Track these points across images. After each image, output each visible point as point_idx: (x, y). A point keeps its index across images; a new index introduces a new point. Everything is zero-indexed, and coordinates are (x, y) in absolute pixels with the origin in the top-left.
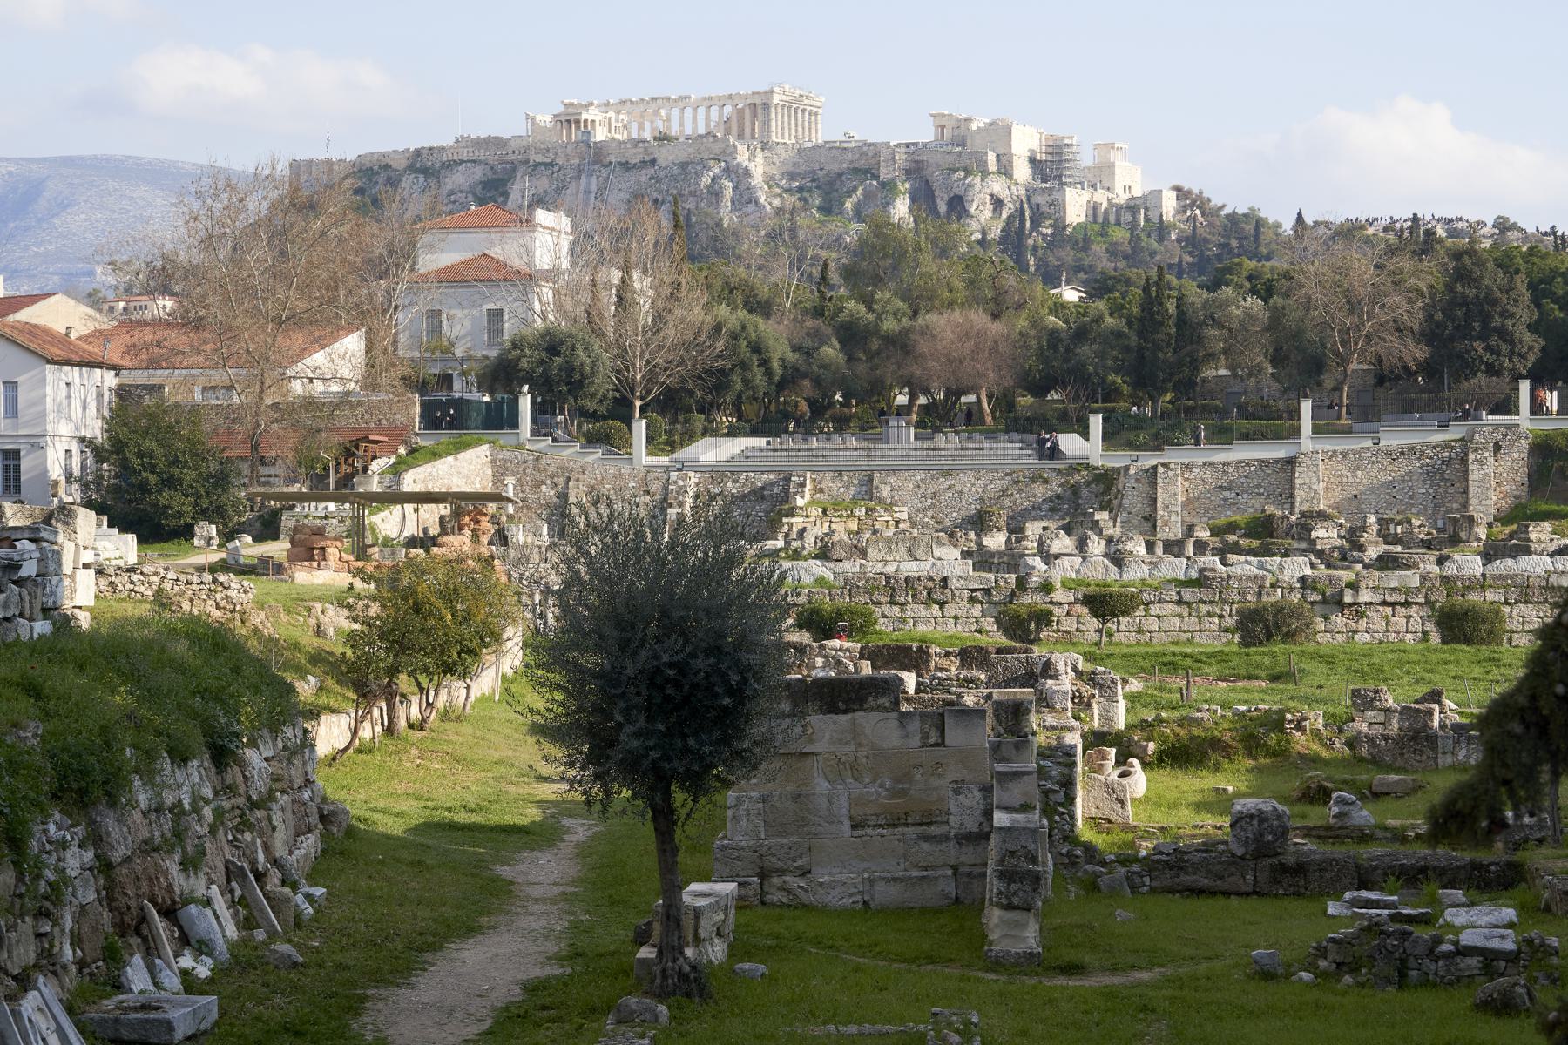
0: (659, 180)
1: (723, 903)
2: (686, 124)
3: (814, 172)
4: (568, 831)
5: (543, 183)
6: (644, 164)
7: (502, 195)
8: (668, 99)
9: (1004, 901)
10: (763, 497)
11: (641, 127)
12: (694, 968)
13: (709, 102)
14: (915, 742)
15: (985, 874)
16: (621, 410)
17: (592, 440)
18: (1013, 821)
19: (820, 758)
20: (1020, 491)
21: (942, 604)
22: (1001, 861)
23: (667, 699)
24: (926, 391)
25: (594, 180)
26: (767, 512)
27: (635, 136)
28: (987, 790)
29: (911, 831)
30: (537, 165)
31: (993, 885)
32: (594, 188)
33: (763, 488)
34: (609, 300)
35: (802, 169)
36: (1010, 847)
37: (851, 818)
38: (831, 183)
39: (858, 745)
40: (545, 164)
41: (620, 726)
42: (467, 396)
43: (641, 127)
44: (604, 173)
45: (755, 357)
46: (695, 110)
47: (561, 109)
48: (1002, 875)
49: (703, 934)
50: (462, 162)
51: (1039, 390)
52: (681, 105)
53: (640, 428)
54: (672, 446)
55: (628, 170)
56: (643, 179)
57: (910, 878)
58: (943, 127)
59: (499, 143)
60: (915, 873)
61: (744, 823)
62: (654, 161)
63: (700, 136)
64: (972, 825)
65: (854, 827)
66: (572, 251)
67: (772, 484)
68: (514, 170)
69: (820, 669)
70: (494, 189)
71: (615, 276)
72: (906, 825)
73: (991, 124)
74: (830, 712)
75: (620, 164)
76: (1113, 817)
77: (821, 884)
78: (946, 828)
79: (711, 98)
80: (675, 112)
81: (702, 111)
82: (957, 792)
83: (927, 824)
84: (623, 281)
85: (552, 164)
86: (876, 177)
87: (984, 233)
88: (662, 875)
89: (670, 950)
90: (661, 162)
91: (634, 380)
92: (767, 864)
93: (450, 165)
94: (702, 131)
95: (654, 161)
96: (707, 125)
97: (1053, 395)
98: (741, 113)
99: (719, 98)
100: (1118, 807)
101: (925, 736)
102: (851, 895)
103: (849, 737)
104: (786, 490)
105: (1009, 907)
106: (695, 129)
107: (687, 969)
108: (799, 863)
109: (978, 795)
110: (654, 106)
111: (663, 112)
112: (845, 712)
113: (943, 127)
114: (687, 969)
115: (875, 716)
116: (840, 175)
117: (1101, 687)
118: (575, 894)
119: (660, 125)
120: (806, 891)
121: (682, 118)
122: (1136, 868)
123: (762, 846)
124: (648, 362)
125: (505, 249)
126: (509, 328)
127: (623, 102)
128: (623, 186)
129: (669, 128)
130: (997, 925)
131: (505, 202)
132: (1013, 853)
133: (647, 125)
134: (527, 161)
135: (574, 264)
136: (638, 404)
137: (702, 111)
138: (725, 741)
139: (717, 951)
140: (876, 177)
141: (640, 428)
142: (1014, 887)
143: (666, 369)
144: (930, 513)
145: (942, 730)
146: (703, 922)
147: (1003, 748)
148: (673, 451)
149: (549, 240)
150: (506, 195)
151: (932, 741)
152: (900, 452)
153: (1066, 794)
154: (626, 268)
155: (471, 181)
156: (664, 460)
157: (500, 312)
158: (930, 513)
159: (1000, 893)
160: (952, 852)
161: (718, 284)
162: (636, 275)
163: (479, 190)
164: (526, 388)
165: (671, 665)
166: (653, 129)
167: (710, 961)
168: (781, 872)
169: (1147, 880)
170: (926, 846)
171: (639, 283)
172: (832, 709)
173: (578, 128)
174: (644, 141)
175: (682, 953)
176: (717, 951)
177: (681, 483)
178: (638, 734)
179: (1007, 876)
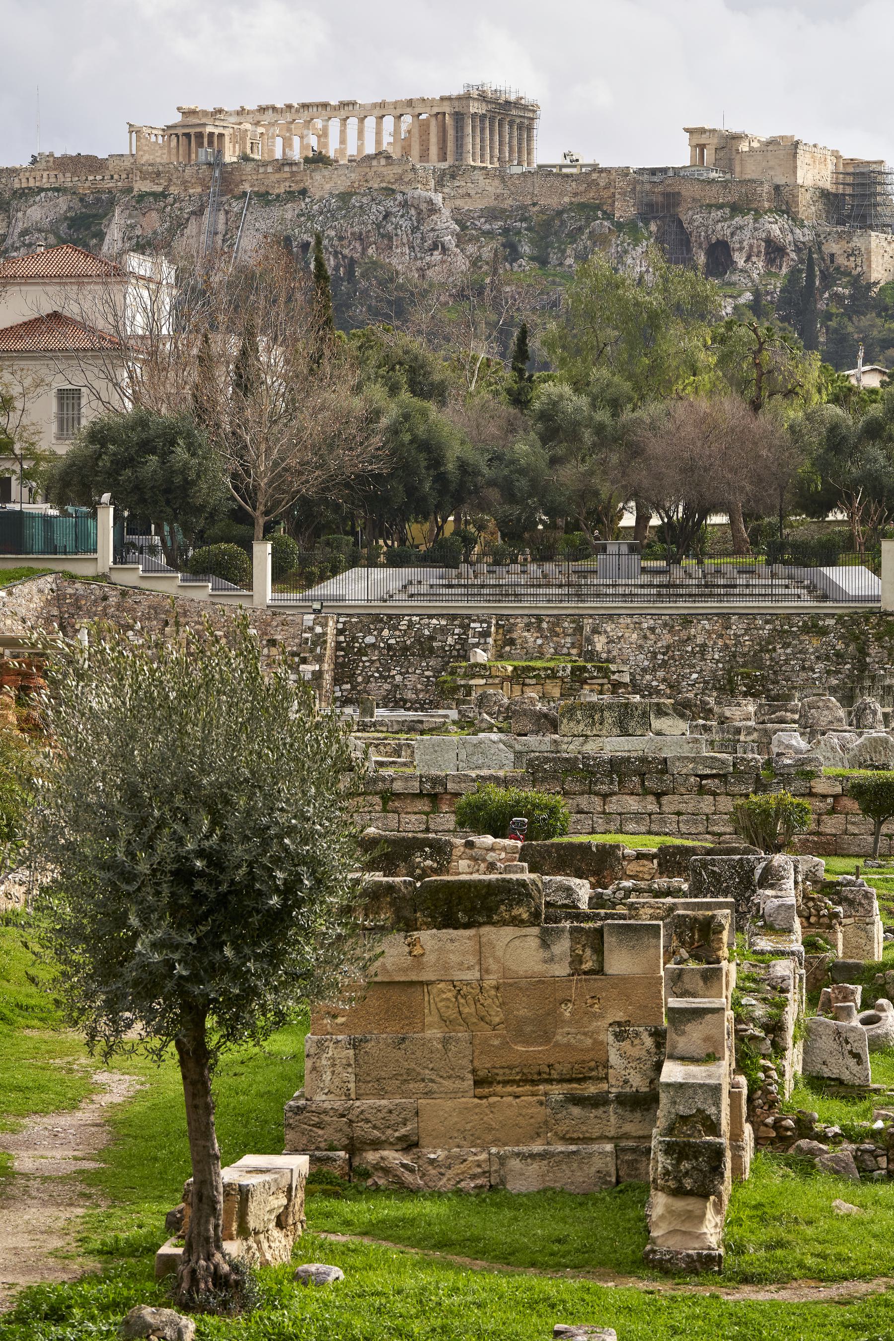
0: (311, 218)
1: (284, 1183)
2: (347, 141)
3: (524, 208)
4: (103, 1088)
5: (152, 223)
6: (291, 196)
7: (95, 236)
8: (325, 105)
9: (672, 1184)
10: (431, 650)
11: (287, 143)
12: (235, 1268)
13: (381, 109)
14: (562, 970)
15: (649, 1150)
16: (240, 527)
17: (198, 570)
18: (688, 1075)
19: (434, 990)
20: (786, 645)
21: (658, 796)
22: (670, 1130)
23: (199, 898)
24: (658, 507)
25: (222, 217)
26: (437, 672)
27: (278, 155)
28: (659, 1036)
29: (557, 1092)
30: (142, 197)
31: (660, 1162)
32: (221, 227)
33: (432, 638)
34: (224, 376)
35: (508, 203)
36: (682, 1110)
37: (474, 1071)
38: (547, 225)
39: (485, 971)
40: (153, 194)
41: (136, 935)
42: (28, 508)
43: (287, 143)
44: (236, 206)
45: (422, 456)
46: (362, 120)
47: (177, 118)
48: (669, 1149)
49: (253, 1223)
50: (41, 190)
51: (817, 506)
52: (343, 113)
53: (263, 554)
54: (310, 581)
55: (268, 203)
56: (289, 216)
57: (552, 1155)
58: (702, 147)
59: (91, 164)
60: (560, 1148)
61: (327, 1077)
62: (304, 192)
63: (369, 158)
64: (638, 1082)
65: (478, 1083)
66: (174, 307)
67: (443, 630)
68: (112, 203)
69: (463, 870)
70: (82, 228)
71: (234, 346)
72: (550, 1081)
73: (769, 143)
74: (446, 926)
75: (258, 194)
76: (846, 1076)
77: (432, 1162)
78: (605, 1086)
79: (382, 105)
80: (334, 125)
81: (370, 122)
82: (620, 1036)
83: (579, 1081)
84: (244, 353)
85: (164, 195)
86: (609, 216)
87: (757, 294)
88: (193, 1141)
89: (201, 1243)
90: (316, 192)
91: (256, 488)
92: (358, 1133)
93: (25, 194)
94: (370, 149)
95: (304, 192)
96: (378, 142)
97: (837, 516)
98: (424, 128)
99: (396, 105)
100: (852, 1062)
101: (577, 960)
102: (474, 1177)
103: (472, 960)
104: (462, 641)
105: (678, 1192)
106: (360, 148)
107: (226, 1268)
108: (403, 1131)
109: (649, 1042)
110: (306, 115)
111: (319, 123)
112: (467, 926)
113: (702, 147)
114: (226, 1268)
115: (508, 932)
116: (560, 213)
117: (851, 903)
118: (98, 1172)
119: (313, 141)
120: (411, 1170)
121: (343, 132)
122: (868, 1146)
123: (351, 1108)
124: (276, 464)
125: (84, 304)
126: (90, 413)
127: (263, 110)
128: (261, 225)
129: (326, 145)
130: (662, 1217)
131: (100, 245)
132: (684, 1119)
133: (296, 140)
134: (130, 190)
135: (178, 328)
136: (261, 521)
137: (370, 122)
138: (274, 958)
139: (277, 1248)
140: (609, 216)
141: (263, 554)
142: (685, 1165)
143: (300, 473)
144: (661, 674)
145: (599, 951)
146: (252, 1206)
147: (686, 978)
148: (309, 586)
149: (144, 298)
150: (101, 236)
151: (586, 966)
152: (621, 590)
153: (774, 1044)
154: (249, 334)
155: (52, 216)
156: (295, 596)
157: (75, 394)
158: (661, 674)
159: (667, 1173)
160: (612, 1120)
161: (374, 357)
162: (262, 341)
163: (63, 228)
164: (106, 497)
165: (201, 853)
166: (303, 147)
167: (265, 1264)
168: (376, 1145)
169: (883, 1162)
170: (576, 1111)
171: (271, 357)
172: (449, 922)
173: (210, 143)
174: (292, 164)
175: (219, 1248)
176: (277, 1248)
177: (319, 630)
178: (155, 946)
179: (678, 1151)
